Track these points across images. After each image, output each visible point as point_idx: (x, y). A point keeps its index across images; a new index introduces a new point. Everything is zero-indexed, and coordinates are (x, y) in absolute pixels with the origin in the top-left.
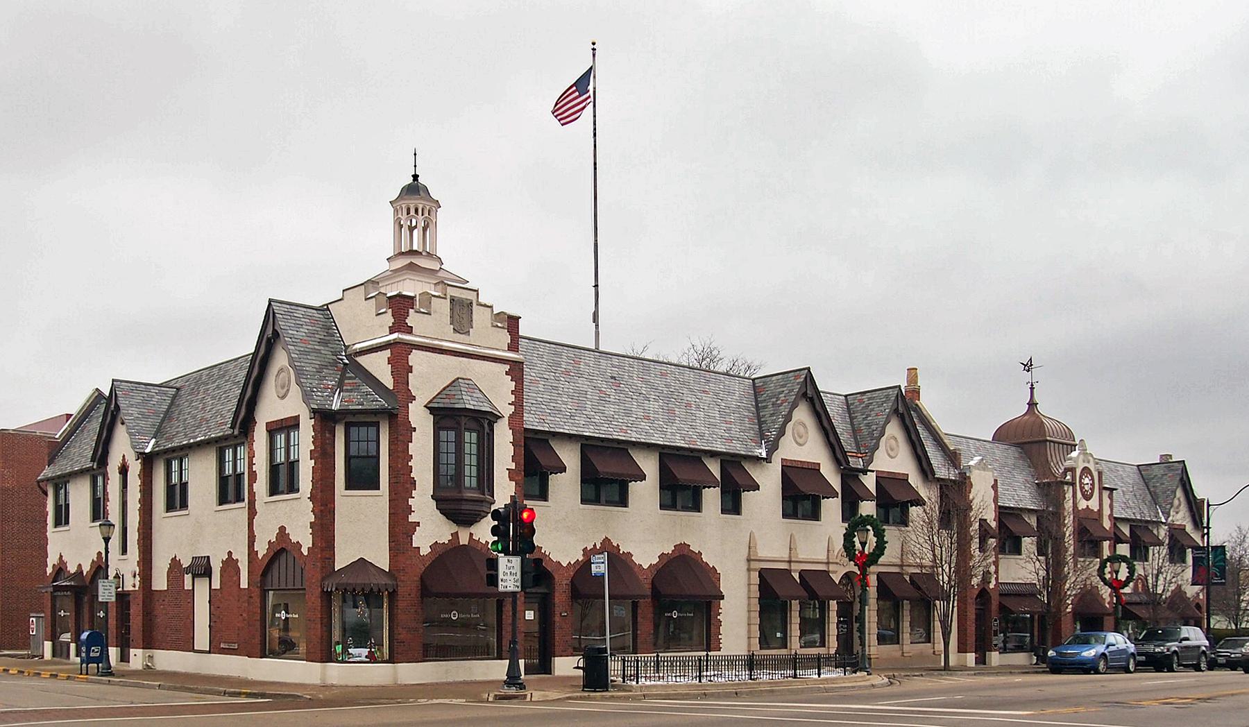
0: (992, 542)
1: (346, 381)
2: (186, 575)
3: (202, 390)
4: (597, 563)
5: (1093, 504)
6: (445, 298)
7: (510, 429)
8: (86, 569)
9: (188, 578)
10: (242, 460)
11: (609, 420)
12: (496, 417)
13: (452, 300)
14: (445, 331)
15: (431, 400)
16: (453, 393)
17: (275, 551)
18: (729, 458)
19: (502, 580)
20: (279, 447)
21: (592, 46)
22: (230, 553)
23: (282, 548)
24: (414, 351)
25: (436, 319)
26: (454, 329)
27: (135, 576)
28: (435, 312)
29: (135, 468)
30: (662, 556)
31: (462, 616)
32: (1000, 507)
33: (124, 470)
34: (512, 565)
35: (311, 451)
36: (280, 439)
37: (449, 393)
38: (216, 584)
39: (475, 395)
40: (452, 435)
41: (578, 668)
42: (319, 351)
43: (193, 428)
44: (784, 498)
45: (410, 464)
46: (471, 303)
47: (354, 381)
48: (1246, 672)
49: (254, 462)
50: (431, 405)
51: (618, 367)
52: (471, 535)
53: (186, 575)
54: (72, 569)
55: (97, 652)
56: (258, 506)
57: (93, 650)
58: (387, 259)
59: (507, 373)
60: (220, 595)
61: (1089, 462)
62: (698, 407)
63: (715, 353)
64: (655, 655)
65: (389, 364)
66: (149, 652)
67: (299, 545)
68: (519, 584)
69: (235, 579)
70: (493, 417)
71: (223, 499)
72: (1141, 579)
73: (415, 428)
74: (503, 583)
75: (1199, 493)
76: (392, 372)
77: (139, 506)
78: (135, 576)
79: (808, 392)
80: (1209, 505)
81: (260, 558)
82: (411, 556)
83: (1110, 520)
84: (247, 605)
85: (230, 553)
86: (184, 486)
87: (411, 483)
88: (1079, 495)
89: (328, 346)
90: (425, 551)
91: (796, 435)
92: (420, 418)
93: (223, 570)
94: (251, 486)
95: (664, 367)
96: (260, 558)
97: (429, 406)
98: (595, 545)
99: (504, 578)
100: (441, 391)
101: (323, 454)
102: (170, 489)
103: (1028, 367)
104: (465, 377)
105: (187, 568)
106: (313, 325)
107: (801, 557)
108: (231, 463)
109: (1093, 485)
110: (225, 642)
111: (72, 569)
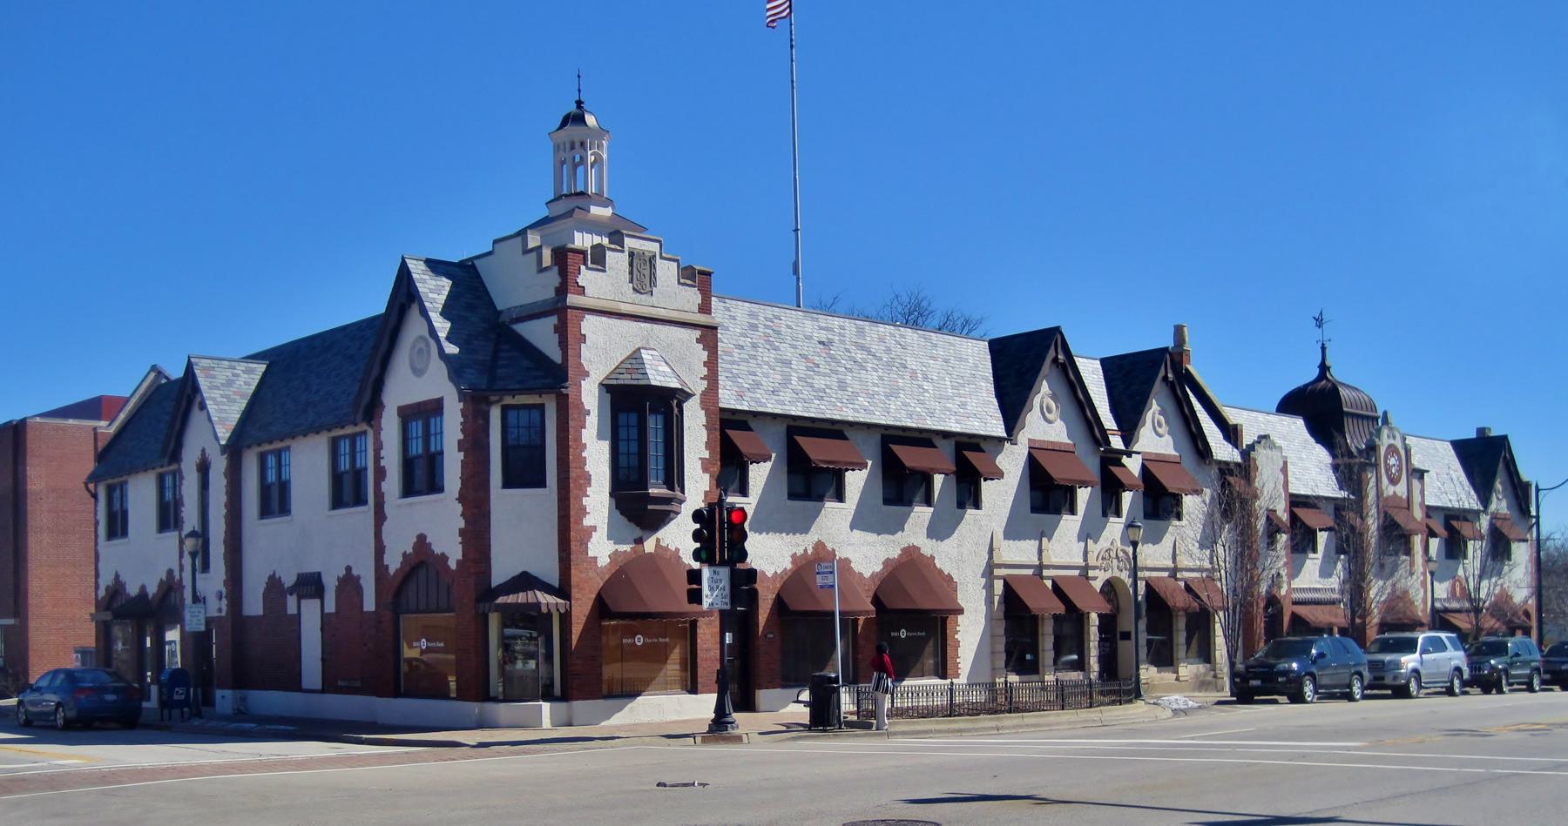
0: (1283, 538)
2: (288, 596)
4: (824, 573)
5: (1401, 489)
6: (623, 252)
8: (152, 590)
9: (291, 602)
12: (688, 396)
13: (631, 255)
16: (635, 366)
18: (965, 440)
19: (706, 596)
20: (414, 435)
22: (349, 569)
23: (422, 559)
24: (586, 316)
25: (612, 277)
26: (634, 289)
27: (220, 599)
29: (219, 464)
30: (887, 562)
32: (1292, 495)
33: (204, 468)
34: (718, 577)
38: (331, 607)
39: (660, 368)
40: (633, 418)
44: (1031, 489)
46: (655, 256)
48: (1565, 688)
49: (382, 456)
50: (606, 382)
52: (658, 540)
53: (288, 596)
54: (133, 590)
55: (182, 694)
56: (388, 509)
57: (177, 692)
58: (547, 204)
59: (698, 341)
61: (1394, 438)
62: (926, 378)
63: (924, 304)
67: (443, 558)
68: (728, 600)
70: (681, 395)
71: (337, 502)
72: (1460, 581)
73: (589, 411)
75: (1525, 474)
78: (220, 599)
79: (1059, 357)
80: (1538, 490)
82: (587, 568)
83: (1422, 509)
85: (349, 569)
86: (284, 487)
87: (585, 479)
88: (1385, 480)
90: (603, 561)
91: (1045, 410)
92: (590, 395)
95: (851, 316)
96: (392, 574)
98: (806, 550)
100: (620, 365)
101: (474, 444)
102: (265, 489)
103: (1319, 322)
107: (1055, 561)
108: (347, 457)
109: (1400, 466)
111: (133, 590)
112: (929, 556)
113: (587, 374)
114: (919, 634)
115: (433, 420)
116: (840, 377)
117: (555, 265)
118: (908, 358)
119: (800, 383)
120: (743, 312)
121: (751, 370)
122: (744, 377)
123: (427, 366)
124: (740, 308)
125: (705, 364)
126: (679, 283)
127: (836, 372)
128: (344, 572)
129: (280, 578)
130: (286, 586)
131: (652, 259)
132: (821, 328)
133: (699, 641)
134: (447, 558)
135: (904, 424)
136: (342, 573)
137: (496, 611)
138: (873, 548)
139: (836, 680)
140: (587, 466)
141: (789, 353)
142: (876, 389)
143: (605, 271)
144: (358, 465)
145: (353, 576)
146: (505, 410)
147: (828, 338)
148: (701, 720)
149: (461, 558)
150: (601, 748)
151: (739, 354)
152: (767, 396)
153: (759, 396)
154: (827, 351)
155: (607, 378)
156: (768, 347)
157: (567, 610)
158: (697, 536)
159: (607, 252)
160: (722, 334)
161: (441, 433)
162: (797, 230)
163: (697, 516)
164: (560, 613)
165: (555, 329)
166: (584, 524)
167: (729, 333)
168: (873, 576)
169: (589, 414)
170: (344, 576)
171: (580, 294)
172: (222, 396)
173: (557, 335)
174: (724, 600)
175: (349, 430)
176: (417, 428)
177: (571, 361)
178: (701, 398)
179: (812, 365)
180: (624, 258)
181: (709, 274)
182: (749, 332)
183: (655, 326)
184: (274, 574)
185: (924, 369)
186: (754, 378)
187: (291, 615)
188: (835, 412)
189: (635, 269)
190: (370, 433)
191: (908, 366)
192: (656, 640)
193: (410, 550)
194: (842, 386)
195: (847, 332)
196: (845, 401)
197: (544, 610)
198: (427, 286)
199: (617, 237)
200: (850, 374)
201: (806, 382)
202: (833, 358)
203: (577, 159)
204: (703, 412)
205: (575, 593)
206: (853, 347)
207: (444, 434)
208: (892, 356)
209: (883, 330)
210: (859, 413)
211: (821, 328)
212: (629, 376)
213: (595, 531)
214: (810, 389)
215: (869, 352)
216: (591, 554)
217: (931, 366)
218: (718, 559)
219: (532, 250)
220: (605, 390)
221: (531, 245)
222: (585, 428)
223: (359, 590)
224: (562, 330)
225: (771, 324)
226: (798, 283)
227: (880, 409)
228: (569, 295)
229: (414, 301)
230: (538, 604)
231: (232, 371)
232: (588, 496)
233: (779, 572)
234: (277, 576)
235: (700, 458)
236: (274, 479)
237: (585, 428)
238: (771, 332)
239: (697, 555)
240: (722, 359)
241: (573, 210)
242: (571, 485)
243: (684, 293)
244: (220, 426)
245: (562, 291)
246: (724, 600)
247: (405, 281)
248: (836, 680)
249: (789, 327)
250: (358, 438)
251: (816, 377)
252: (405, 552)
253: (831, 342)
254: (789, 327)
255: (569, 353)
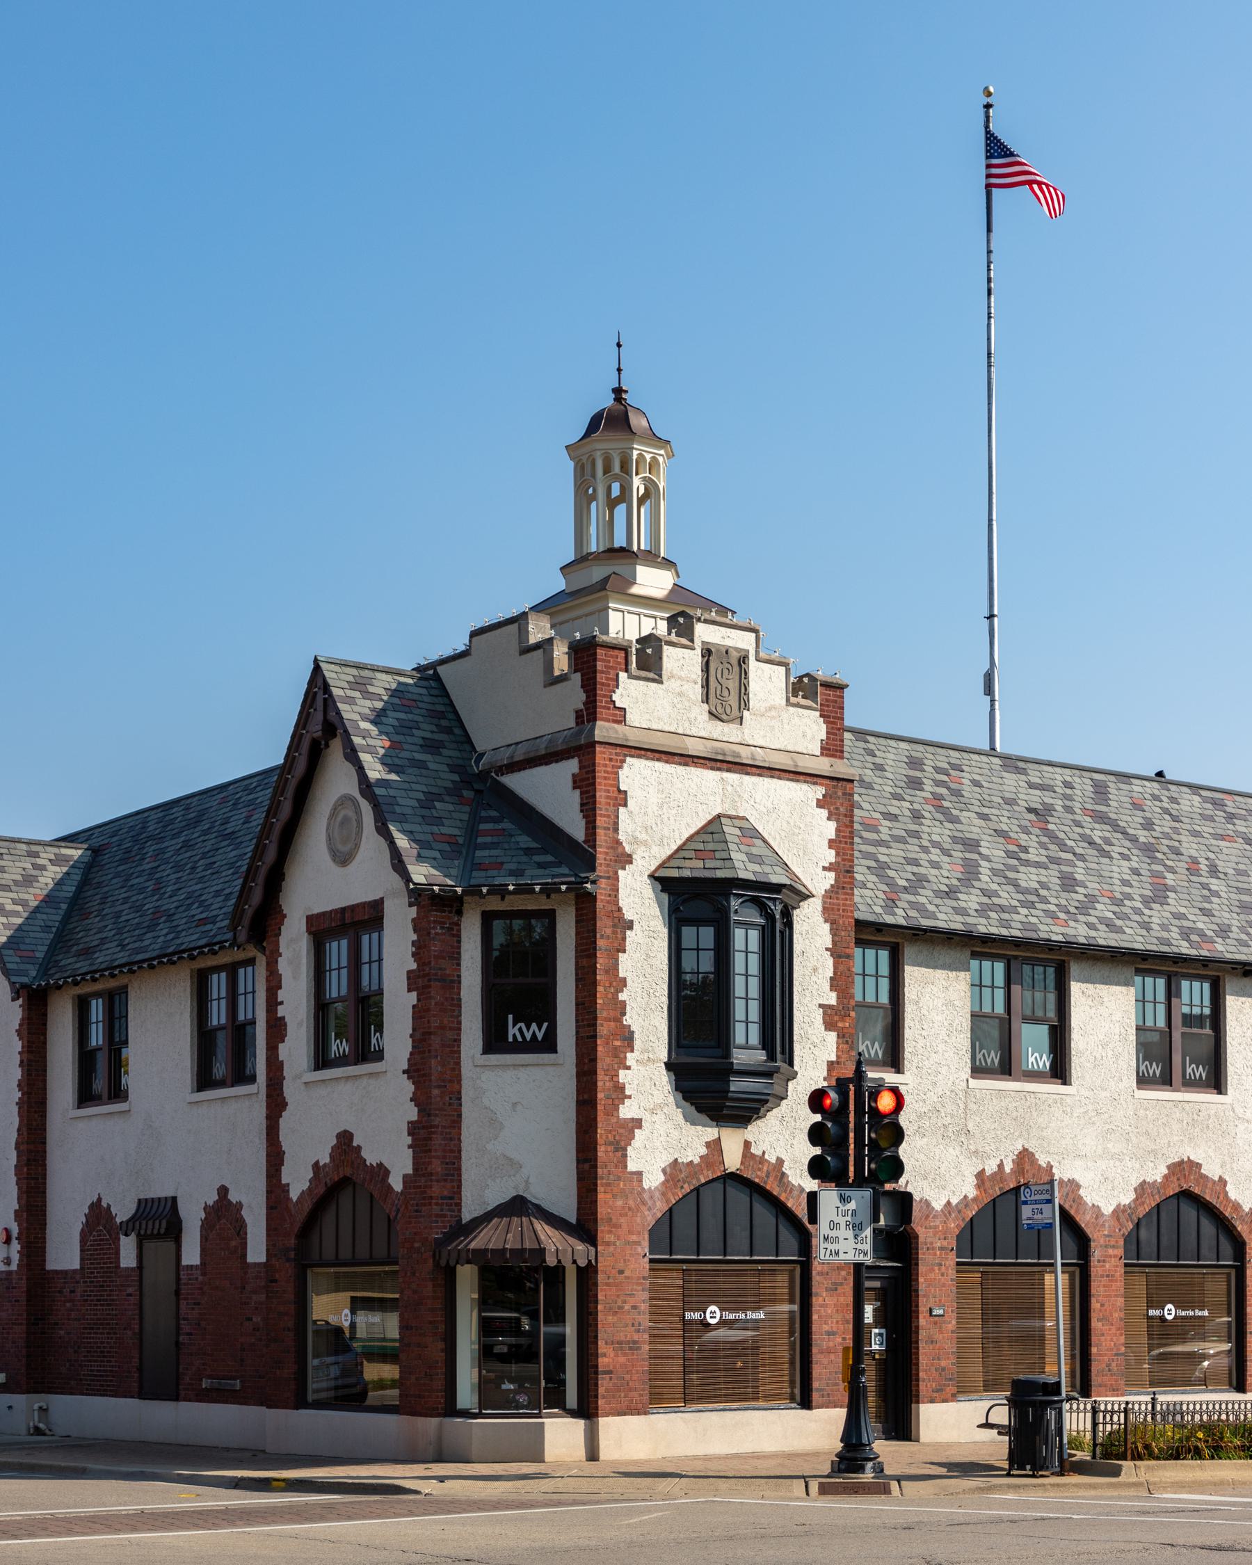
1: (482, 826)
2: (122, 1237)
3: (151, 848)
4: (1036, 1202)
11: (1031, 898)
12: (805, 897)
13: (707, 652)
16: (710, 846)
20: (335, 965)
21: (985, 100)
22: (223, 1191)
24: (628, 759)
27: (8, 1241)
28: (672, 676)
30: (1142, 1189)
31: (1182, 1313)
36: (338, 950)
37: (701, 846)
40: (707, 935)
41: (987, 1425)
42: (422, 765)
43: (137, 932)
45: (622, 997)
51: (1042, 787)
52: (747, 1144)
53: (122, 1237)
56: (290, 1090)
58: (562, 569)
59: (820, 804)
60: (200, 1278)
62: (1214, 871)
64: (1148, 1398)
65: (574, 788)
66: (39, 1400)
67: (381, 1172)
69: (233, 1243)
71: (204, 1080)
73: (632, 922)
74: (830, 1246)
76: (582, 805)
77: (20, 1094)
78: (8, 1241)
81: (295, 1199)
85: (223, 1191)
86: (117, 1065)
90: (653, 1179)
93: (207, 1226)
94: (272, 1049)
96: (295, 1199)
98: (1001, 1166)
99: (833, 1234)
100: (684, 844)
102: (86, 1059)
106: (407, 709)
110: (210, 1377)
112: (1216, 1179)
113: (627, 859)
114: (1198, 1313)
115: (365, 938)
116: (1064, 868)
118: (1182, 838)
119: (995, 879)
120: (899, 758)
121: (910, 855)
122: (898, 867)
123: (357, 846)
124: (894, 751)
125: (831, 844)
126: (788, 702)
127: (1057, 861)
129: (109, 1206)
130: (118, 1220)
131: (743, 660)
132: (1032, 786)
133: (815, 1317)
134: (387, 1173)
135: (1175, 950)
136: (212, 1198)
137: (469, 1262)
138: (1118, 1163)
141: (972, 826)
142: (1127, 890)
143: (661, 683)
144: (241, 1017)
145: (230, 1203)
146: (488, 919)
147: (1043, 804)
148: (816, 1454)
149: (411, 1172)
150: (644, 1500)
151: (890, 829)
152: (938, 901)
153: (922, 900)
154: (1042, 825)
157: (590, 1261)
158: (816, 1135)
159: (665, 647)
160: (860, 795)
161: (380, 960)
162: (991, 617)
165: (575, 782)
166: (622, 1115)
167: (871, 792)
168: (1119, 1212)
170: (216, 1202)
171: (619, 722)
172: (15, 902)
175: (224, 958)
176: (338, 950)
178: (824, 903)
179: (1015, 849)
181: (841, 688)
182: (908, 791)
183: (746, 778)
184: (99, 1199)
185: (1212, 856)
186: (915, 869)
187: (127, 1269)
188: (1054, 928)
189: (712, 679)
190: (261, 961)
191: (1183, 851)
192: (743, 1316)
193: (325, 1159)
194: (1069, 883)
195: (1079, 793)
196: (1072, 910)
197: (551, 1261)
198: (355, 708)
199: (682, 625)
200: (1079, 864)
202: (1053, 837)
204: (827, 926)
205: (604, 1234)
206: (1089, 819)
208: (1154, 834)
209: (1139, 789)
210: (1097, 930)
211: (1032, 786)
212: (700, 864)
213: (640, 1127)
214: (1010, 888)
215: (1115, 826)
216: (632, 1166)
217: (1225, 851)
219: (538, 646)
220: (660, 887)
221: (534, 638)
222: (624, 951)
223: (240, 1228)
224: (585, 784)
225: (945, 778)
227: (1135, 925)
228: (599, 723)
229: (335, 736)
231: (33, 860)
232: (629, 1068)
233: (954, 1201)
235: (821, 1006)
236: (101, 1042)
237: (624, 951)
239: (817, 1168)
240: (861, 837)
243: (797, 719)
244: (11, 952)
245: (588, 715)
246: (859, 1246)
247: (320, 697)
249: (976, 783)
250: (241, 971)
251: (1022, 869)
253: (1049, 809)
254: (976, 783)
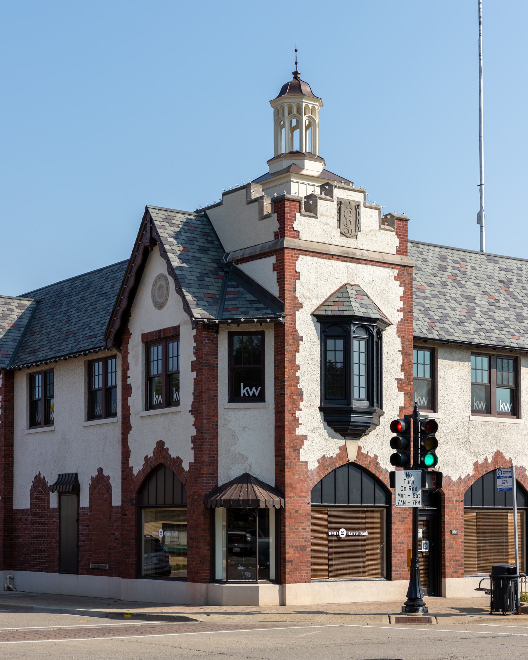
1: (228, 290)
2: (51, 493)
3: (65, 301)
4: (504, 477)
7: (399, 337)
10: (114, 374)
11: (501, 325)
12: (388, 324)
14: (332, 235)
15: (318, 308)
16: (341, 300)
17: (153, 467)
20: (155, 358)
22: (100, 470)
24: (301, 256)
35: (192, 362)
36: (157, 351)
37: (336, 300)
40: (340, 343)
41: (480, 589)
42: (199, 259)
47: (236, 290)
50: (318, 313)
52: (359, 448)
53: (51, 493)
56: (133, 420)
58: (267, 162)
59: (396, 278)
60: (89, 514)
67: (178, 461)
69: (105, 496)
71: (91, 415)
73: (302, 337)
76: (278, 279)
84: (120, 523)
85: (100, 470)
86: (48, 408)
89: (208, 254)
90: (313, 465)
93: (93, 488)
96: (136, 474)
97: (315, 314)
98: (486, 459)
100: (328, 298)
102: (33, 405)
104: (352, 283)
105: (54, 485)
106: (191, 231)
110: (94, 562)
113: (300, 306)
115: (171, 345)
117: (274, 213)
119: (483, 316)
123: (167, 299)
125: (401, 298)
127: (514, 307)
128: (97, 473)
129: (44, 477)
130: (49, 485)
131: (357, 207)
132: (501, 269)
133: (393, 534)
134: (181, 461)
136: (95, 474)
139: (514, 571)
140: (300, 384)
141: (471, 289)
143: (317, 218)
145: (104, 476)
146: (231, 335)
147: (507, 278)
148: (394, 603)
149: (193, 461)
151: (431, 291)
152: (455, 327)
154: (506, 289)
155: (317, 309)
156: (455, 285)
158: (394, 443)
159: (319, 201)
160: (416, 274)
163: (394, 426)
164: (276, 509)
165: (274, 267)
166: (297, 433)
167: (421, 272)
169: (302, 340)
170: (97, 476)
171: (296, 238)
173: (275, 272)
174: (416, 499)
176: (157, 351)
177: (287, 295)
178: (398, 328)
179: (493, 301)
180: (333, 206)
181: (406, 220)
183: (359, 265)
184: (40, 474)
186: (443, 311)
187: (53, 509)
188: (513, 341)
189: (342, 216)
193: (151, 455)
196: (522, 331)
198: (166, 231)
201: (488, 315)
202: (512, 295)
203: (294, 123)
204: (399, 339)
205: (288, 492)
207: (180, 357)
211: (501, 269)
212: (336, 308)
216: (302, 459)
218: (412, 463)
219: (256, 200)
220: (316, 320)
221: (254, 196)
222: (299, 352)
223: (109, 488)
225: (458, 265)
226: (481, 231)
228: (286, 238)
229: (156, 245)
230: (257, 501)
231: (7, 306)
232: (301, 410)
234: (42, 476)
235: (396, 379)
236: (40, 396)
238: (457, 272)
239: (394, 460)
241: (291, 165)
242: (286, 400)
245: (280, 234)
246: (416, 499)
247: (148, 228)
248: (514, 571)
249: (473, 268)
250: (109, 361)
251: (496, 311)
252: (147, 456)
253: (510, 281)
254: (473, 268)
255: (286, 288)
